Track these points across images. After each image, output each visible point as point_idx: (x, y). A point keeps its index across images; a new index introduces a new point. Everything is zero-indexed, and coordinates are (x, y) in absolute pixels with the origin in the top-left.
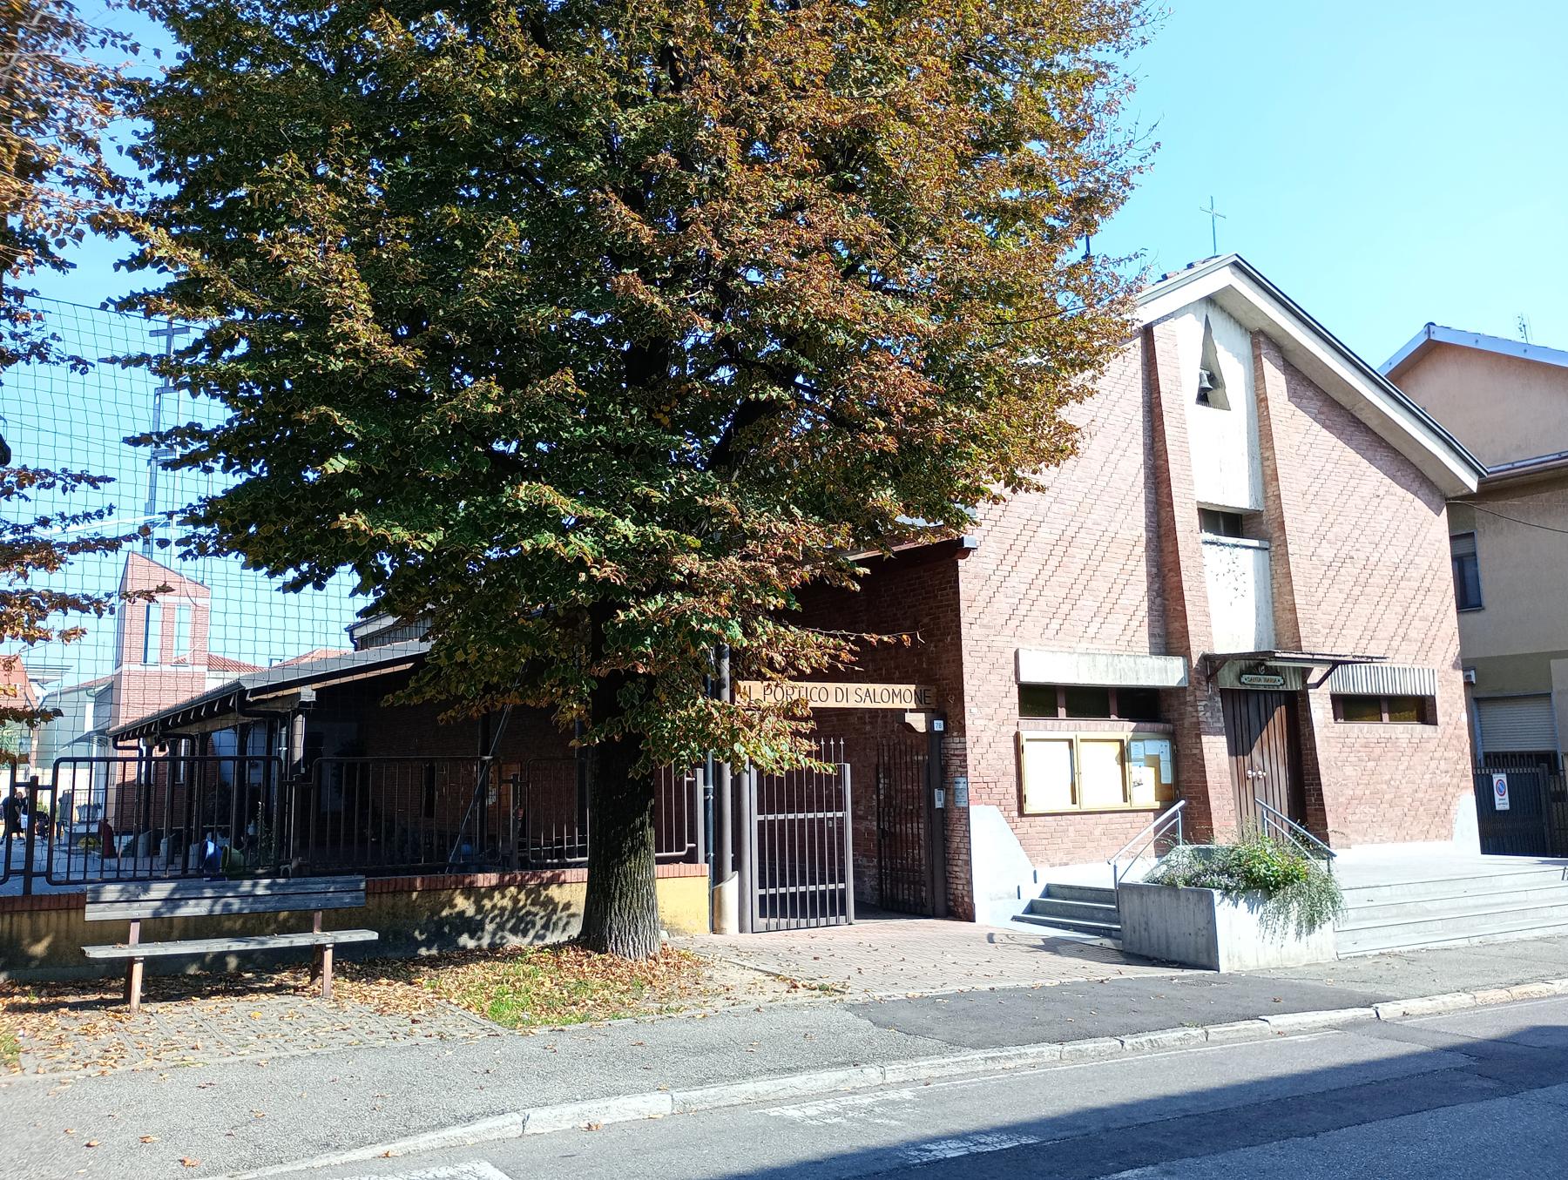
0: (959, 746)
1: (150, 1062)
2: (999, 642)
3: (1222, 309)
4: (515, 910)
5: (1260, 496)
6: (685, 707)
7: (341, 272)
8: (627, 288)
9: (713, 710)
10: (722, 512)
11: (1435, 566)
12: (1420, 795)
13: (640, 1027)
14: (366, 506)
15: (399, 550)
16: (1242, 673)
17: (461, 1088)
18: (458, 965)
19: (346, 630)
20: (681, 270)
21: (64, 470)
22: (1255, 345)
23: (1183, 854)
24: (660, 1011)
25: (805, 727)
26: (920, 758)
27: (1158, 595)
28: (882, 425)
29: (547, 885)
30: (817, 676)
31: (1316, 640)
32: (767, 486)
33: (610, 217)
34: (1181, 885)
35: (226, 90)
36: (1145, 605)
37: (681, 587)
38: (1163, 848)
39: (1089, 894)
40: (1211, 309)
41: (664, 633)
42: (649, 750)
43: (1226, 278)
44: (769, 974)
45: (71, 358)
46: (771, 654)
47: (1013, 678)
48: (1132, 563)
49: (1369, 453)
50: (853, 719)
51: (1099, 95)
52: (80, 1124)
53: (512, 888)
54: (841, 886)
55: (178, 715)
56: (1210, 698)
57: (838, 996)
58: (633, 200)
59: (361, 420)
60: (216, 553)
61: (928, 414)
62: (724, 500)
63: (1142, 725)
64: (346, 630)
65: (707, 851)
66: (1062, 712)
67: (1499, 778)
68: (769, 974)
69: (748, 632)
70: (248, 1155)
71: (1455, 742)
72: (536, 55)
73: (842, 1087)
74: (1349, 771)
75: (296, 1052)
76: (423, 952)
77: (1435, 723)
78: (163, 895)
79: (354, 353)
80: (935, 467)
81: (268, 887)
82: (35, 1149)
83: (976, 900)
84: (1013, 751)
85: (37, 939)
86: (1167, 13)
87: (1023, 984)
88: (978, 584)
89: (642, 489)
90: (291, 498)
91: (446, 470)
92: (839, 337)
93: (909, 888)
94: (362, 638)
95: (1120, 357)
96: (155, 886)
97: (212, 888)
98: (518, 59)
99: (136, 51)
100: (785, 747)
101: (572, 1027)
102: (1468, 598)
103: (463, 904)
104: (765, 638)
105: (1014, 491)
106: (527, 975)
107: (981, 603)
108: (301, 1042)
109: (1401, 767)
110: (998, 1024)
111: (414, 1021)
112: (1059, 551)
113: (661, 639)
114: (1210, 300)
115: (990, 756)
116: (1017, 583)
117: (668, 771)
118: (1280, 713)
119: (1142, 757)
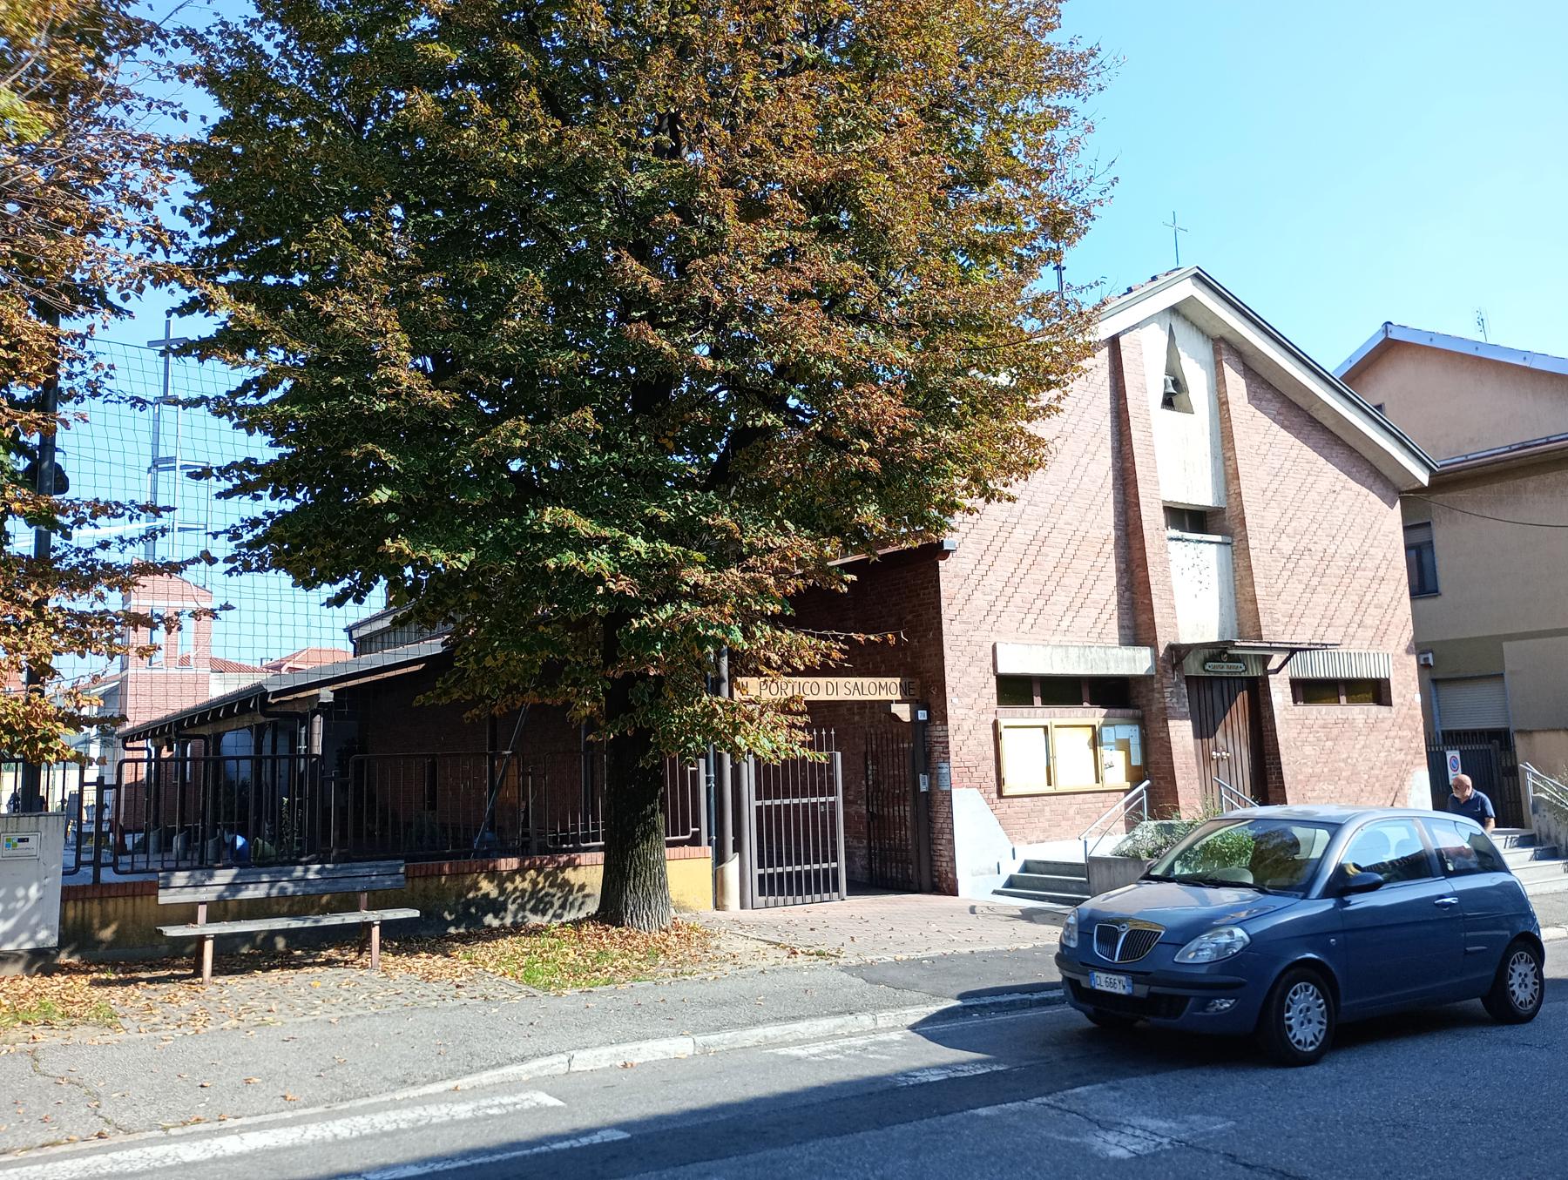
0: (942, 734)
1: (235, 1022)
2: (978, 637)
3: (1185, 318)
4: (534, 893)
5: (1222, 494)
6: (691, 704)
7: (384, 325)
8: (639, 335)
9: (718, 707)
10: (723, 529)
11: (1389, 556)
12: (1376, 772)
13: (659, 988)
14: (411, 533)
15: (421, 565)
16: (1206, 661)
17: (512, 1037)
18: (486, 940)
19: (345, 630)
20: (684, 315)
21: (132, 502)
22: (1216, 351)
23: (1148, 830)
24: (675, 975)
25: (800, 721)
26: (906, 745)
27: (1127, 590)
28: (866, 446)
29: (563, 869)
30: (810, 672)
31: (1276, 629)
32: (761, 499)
33: (623, 270)
34: (1144, 857)
35: (270, 155)
36: (1115, 599)
37: (686, 596)
38: (1131, 825)
39: (1063, 869)
40: (1174, 318)
41: (672, 638)
42: (659, 743)
43: (1186, 289)
44: (770, 943)
45: (132, 398)
46: (768, 654)
47: (991, 670)
48: (1101, 560)
49: (1326, 451)
50: (843, 711)
51: (1060, 136)
52: (190, 1070)
53: (532, 872)
54: (834, 865)
55: (194, 717)
56: (1176, 685)
57: (833, 960)
58: (641, 252)
59: (402, 454)
60: (258, 569)
61: (907, 436)
62: (726, 519)
63: (1113, 711)
64: (345, 630)
65: (709, 834)
66: (1037, 700)
67: (1453, 755)
68: (770, 943)
69: (748, 635)
70: (338, 1091)
71: (1409, 722)
72: (554, 126)
73: (839, 1032)
74: (1308, 750)
75: (360, 1012)
76: (452, 930)
77: (1390, 704)
78: (227, 880)
79: (397, 395)
80: (915, 483)
81: (318, 872)
82: (158, 1089)
83: (958, 876)
84: (992, 738)
85: (104, 925)
86: (1121, 60)
87: (1000, 948)
88: (958, 582)
89: (653, 510)
90: (337, 524)
91: (479, 498)
92: (826, 367)
93: (897, 867)
94: (361, 639)
95: (1084, 377)
96: (218, 872)
97: (269, 873)
98: (537, 129)
99: (185, 120)
100: (781, 739)
101: (599, 989)
102: (1423, 584)
103: (487, 887)
104: (763, 641)
105: (988, 501)
106: (553, 947)
107: (960, 600)
108: (362, 1004)
109: (1358, 746)
110: (976, 979)
111: (458, 986)
112: (1033, 549)
113: (670, 642)
114: (1174, 310)
115: (971, 742)
116: (994, 581)
117: (673, 761)
118: (1242, 698)
119: (1113, 741)
